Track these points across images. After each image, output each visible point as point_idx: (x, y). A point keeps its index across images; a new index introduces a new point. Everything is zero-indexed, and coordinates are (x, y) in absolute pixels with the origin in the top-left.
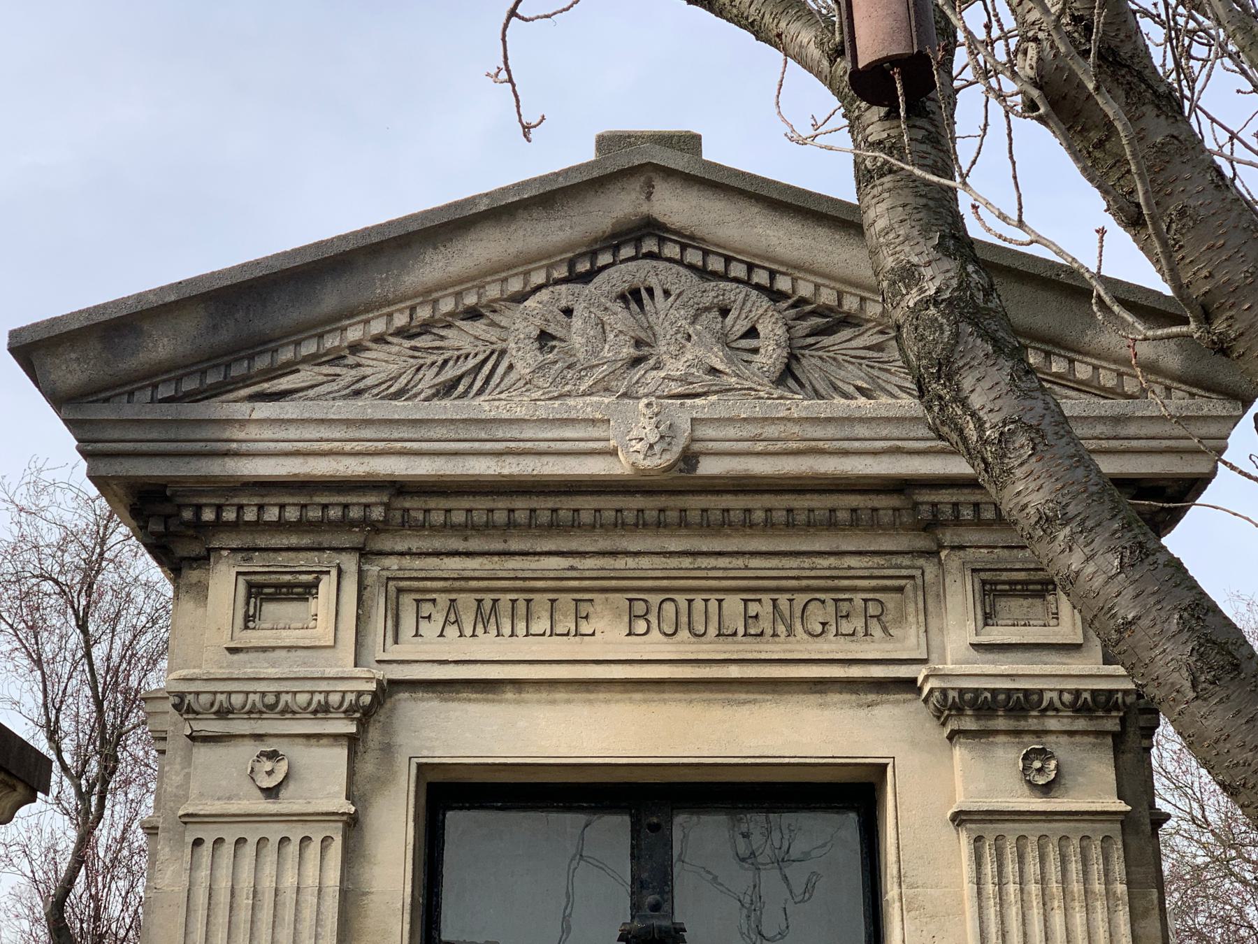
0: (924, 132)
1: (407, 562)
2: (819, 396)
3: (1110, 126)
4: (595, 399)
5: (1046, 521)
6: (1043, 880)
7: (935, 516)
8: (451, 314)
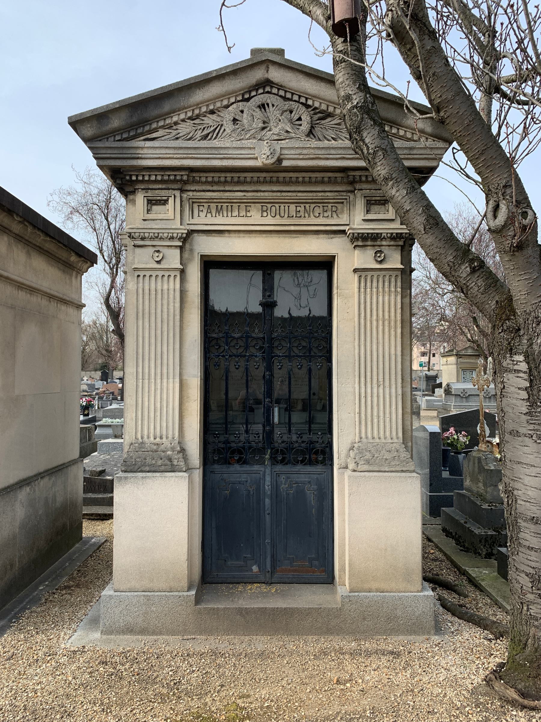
0: (355, 47)
1: (195, 193)
2: (320, 140)
3: (413, 43)
4: (251, 141)
5: (386, 179)
6: (377, 287)
7: (354, 179)
8: (205, 112)
